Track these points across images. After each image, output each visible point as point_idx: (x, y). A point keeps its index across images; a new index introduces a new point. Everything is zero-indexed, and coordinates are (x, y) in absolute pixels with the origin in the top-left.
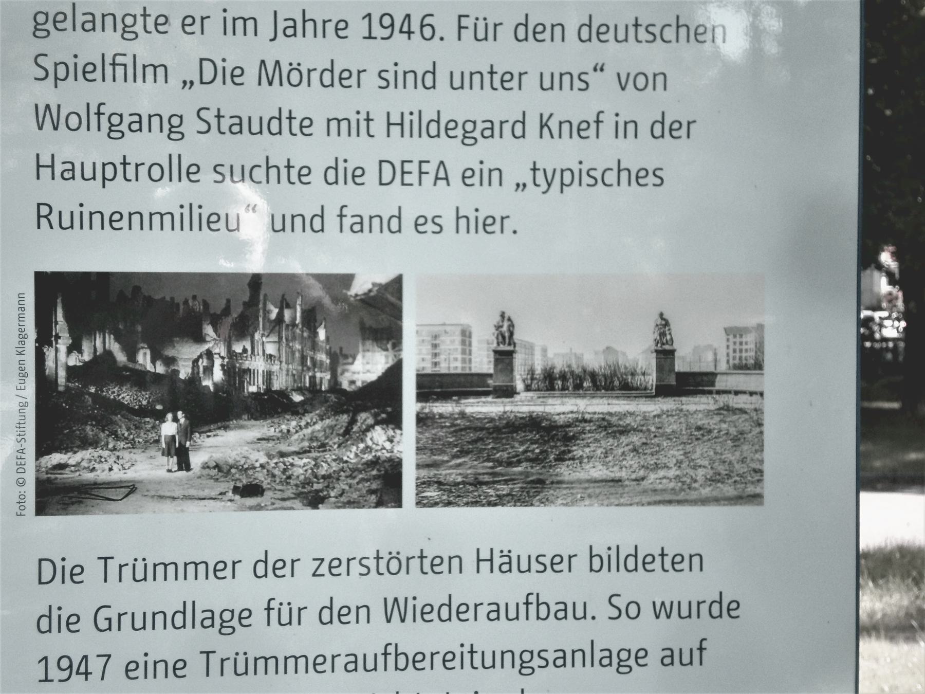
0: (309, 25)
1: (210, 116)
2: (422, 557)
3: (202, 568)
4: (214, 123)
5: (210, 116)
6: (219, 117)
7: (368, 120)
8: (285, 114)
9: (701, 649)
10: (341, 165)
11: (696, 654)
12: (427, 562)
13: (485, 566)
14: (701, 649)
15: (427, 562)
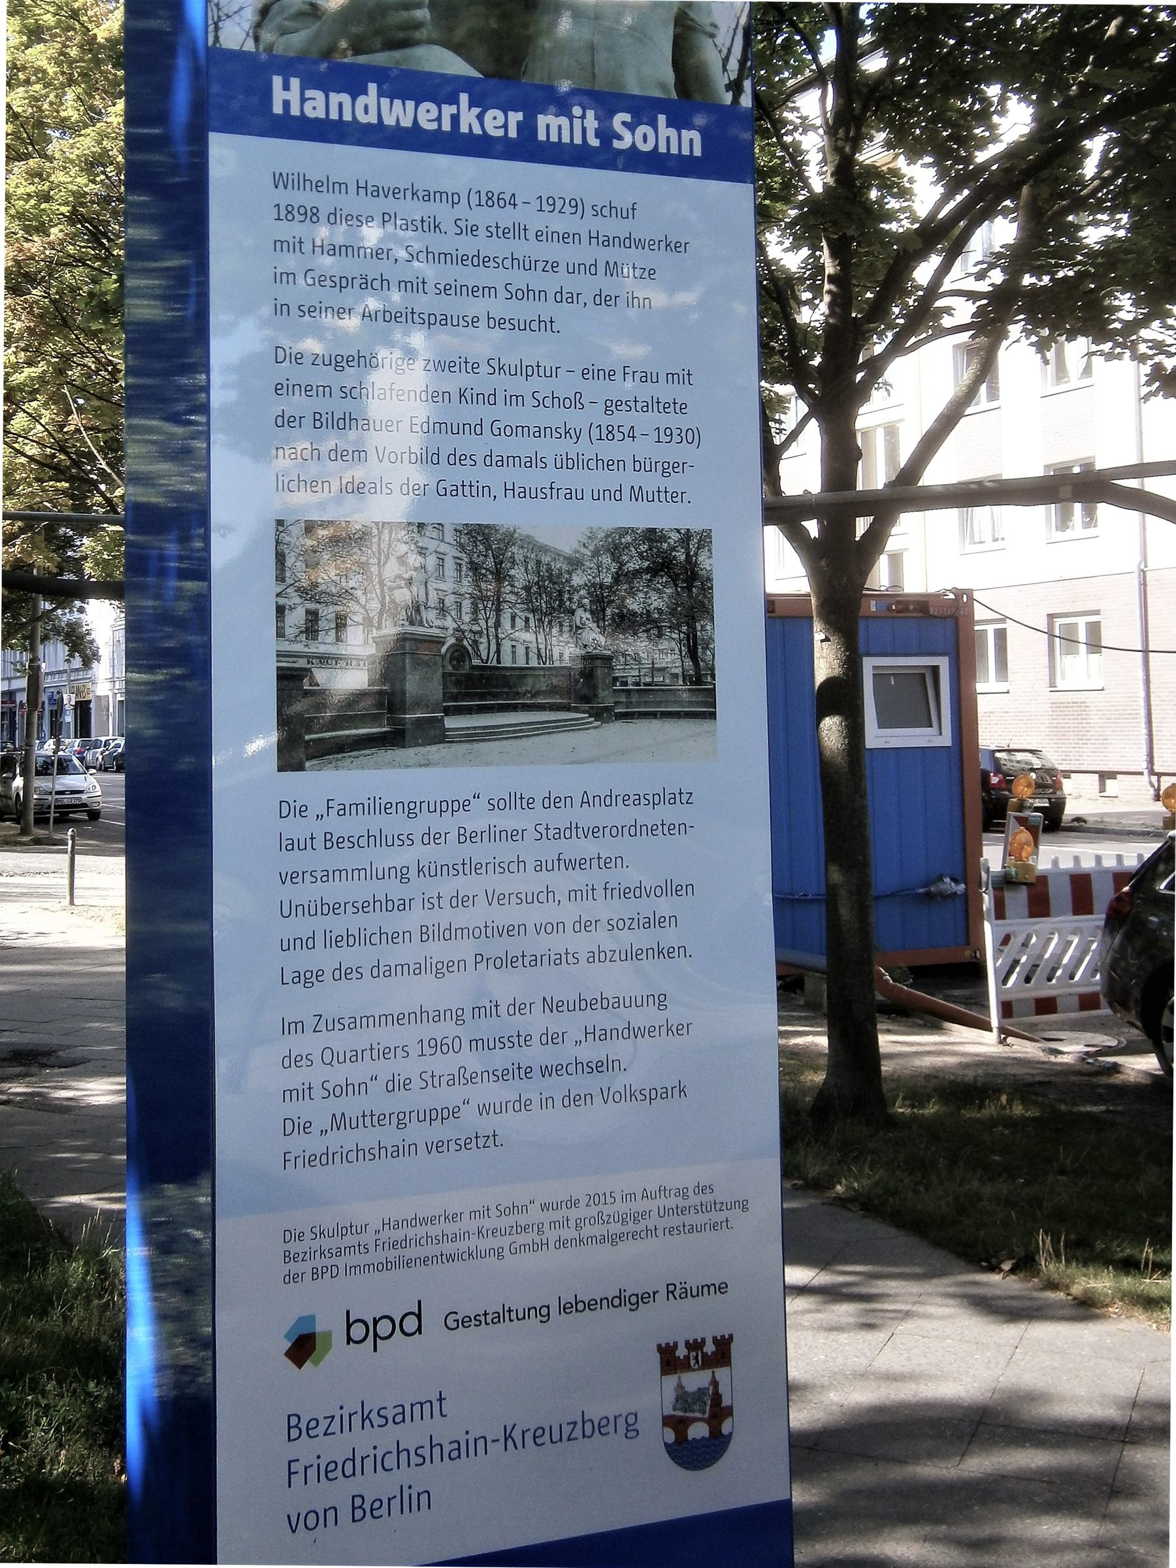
0: (531, 293)
1: (541, 829)
2: (599, 858)
3: (712, 1288)
4: (544, 832)
5: (541, 829)
6: (547, 829)
7: (593, 889)
8: (574, 825)
9: (633, 209)
10: (623, 1294)
11: (630, 212)
12: (602, 861)
13: (594, 241)
14: (633, 209)
15: (602, 861)
